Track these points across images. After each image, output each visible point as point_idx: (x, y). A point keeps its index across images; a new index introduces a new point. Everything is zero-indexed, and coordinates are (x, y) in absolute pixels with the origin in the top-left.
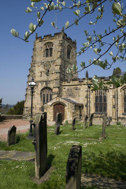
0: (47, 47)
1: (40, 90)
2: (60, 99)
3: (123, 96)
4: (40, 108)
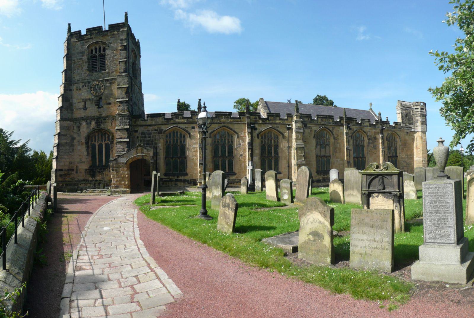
4: (86, 170)
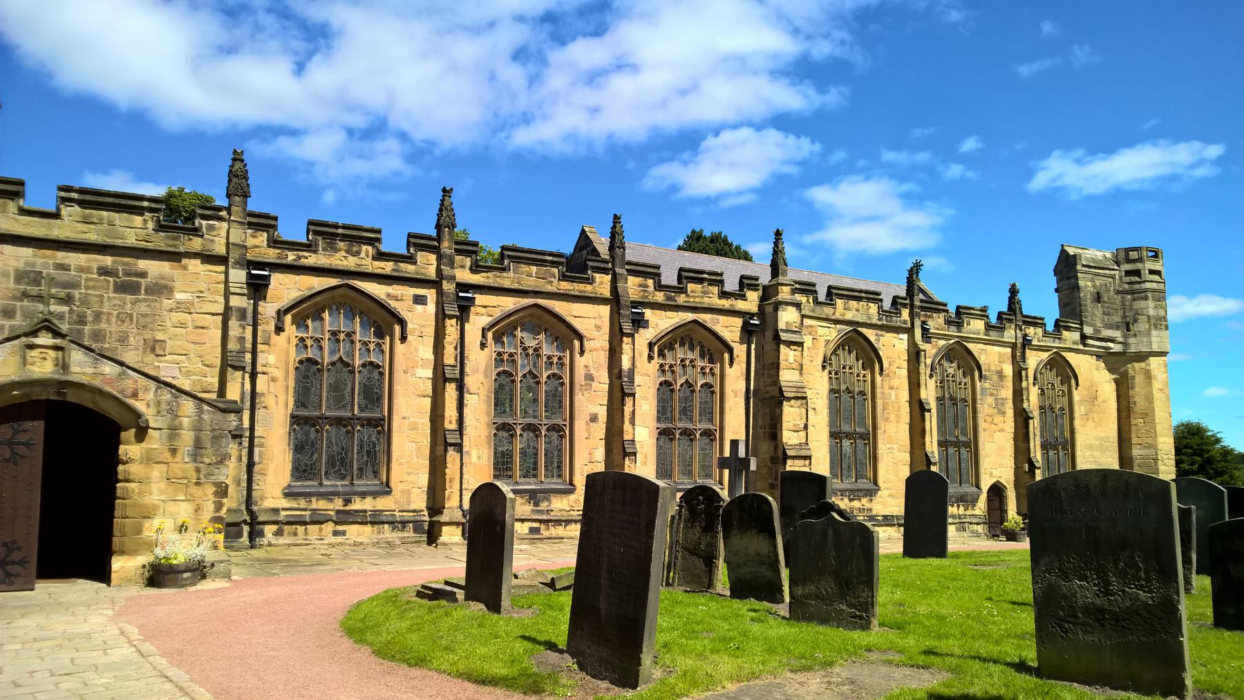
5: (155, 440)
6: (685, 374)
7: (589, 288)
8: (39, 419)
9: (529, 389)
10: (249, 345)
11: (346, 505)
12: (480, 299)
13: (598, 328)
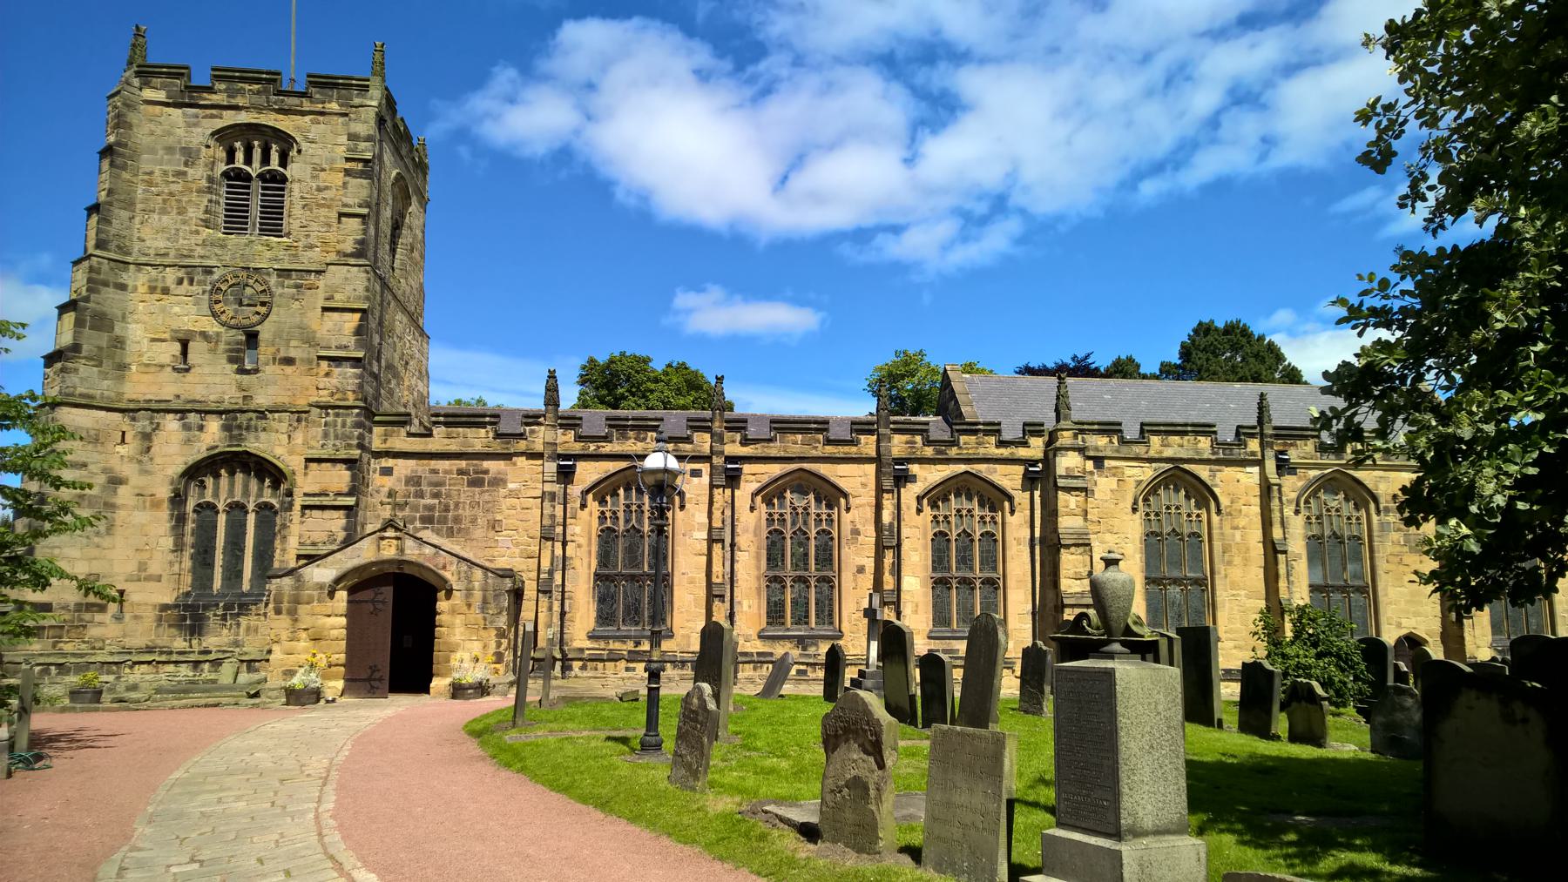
0: (240, 156)
1: (177, 467)
2: (409, 543)
3: (765, 534)
4: (165, 607)
5: (458, 598)
6: (962, 524)
7: (854, 449)
8: (389, 585)
9: (800, 544)
10: (560, 519)
11: (636, 647)
12: (747, 468)
13: (864, 485)
